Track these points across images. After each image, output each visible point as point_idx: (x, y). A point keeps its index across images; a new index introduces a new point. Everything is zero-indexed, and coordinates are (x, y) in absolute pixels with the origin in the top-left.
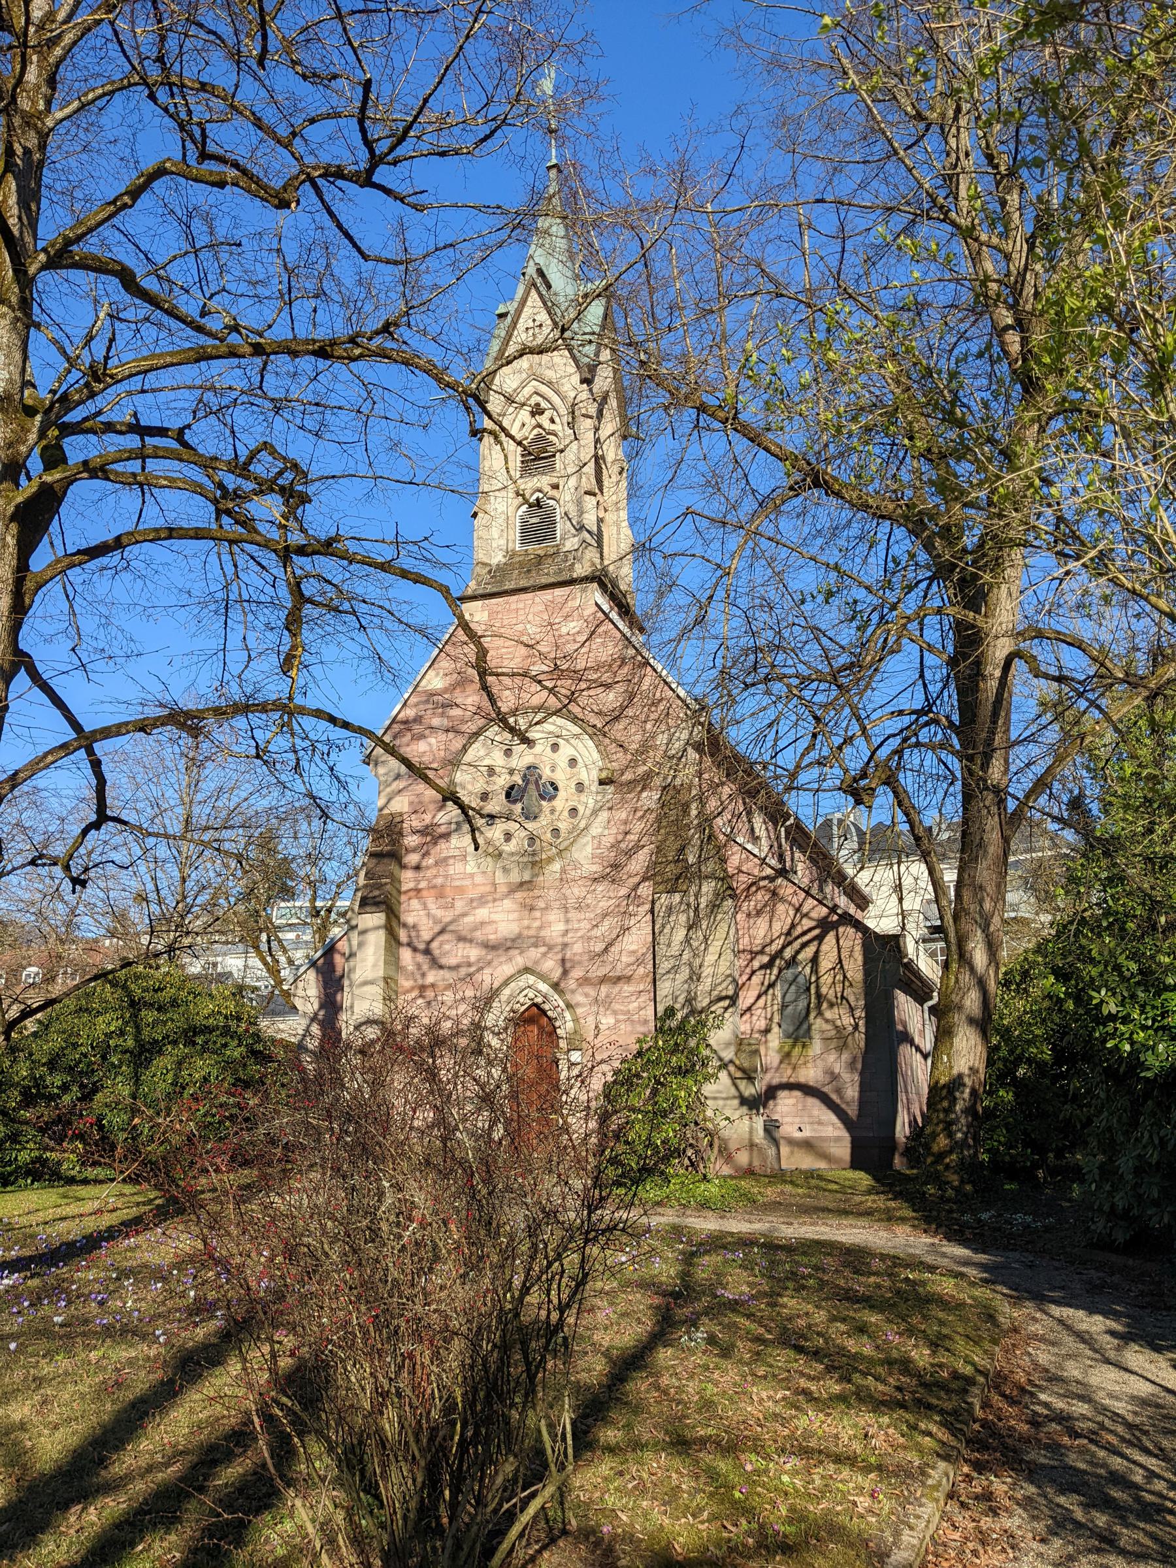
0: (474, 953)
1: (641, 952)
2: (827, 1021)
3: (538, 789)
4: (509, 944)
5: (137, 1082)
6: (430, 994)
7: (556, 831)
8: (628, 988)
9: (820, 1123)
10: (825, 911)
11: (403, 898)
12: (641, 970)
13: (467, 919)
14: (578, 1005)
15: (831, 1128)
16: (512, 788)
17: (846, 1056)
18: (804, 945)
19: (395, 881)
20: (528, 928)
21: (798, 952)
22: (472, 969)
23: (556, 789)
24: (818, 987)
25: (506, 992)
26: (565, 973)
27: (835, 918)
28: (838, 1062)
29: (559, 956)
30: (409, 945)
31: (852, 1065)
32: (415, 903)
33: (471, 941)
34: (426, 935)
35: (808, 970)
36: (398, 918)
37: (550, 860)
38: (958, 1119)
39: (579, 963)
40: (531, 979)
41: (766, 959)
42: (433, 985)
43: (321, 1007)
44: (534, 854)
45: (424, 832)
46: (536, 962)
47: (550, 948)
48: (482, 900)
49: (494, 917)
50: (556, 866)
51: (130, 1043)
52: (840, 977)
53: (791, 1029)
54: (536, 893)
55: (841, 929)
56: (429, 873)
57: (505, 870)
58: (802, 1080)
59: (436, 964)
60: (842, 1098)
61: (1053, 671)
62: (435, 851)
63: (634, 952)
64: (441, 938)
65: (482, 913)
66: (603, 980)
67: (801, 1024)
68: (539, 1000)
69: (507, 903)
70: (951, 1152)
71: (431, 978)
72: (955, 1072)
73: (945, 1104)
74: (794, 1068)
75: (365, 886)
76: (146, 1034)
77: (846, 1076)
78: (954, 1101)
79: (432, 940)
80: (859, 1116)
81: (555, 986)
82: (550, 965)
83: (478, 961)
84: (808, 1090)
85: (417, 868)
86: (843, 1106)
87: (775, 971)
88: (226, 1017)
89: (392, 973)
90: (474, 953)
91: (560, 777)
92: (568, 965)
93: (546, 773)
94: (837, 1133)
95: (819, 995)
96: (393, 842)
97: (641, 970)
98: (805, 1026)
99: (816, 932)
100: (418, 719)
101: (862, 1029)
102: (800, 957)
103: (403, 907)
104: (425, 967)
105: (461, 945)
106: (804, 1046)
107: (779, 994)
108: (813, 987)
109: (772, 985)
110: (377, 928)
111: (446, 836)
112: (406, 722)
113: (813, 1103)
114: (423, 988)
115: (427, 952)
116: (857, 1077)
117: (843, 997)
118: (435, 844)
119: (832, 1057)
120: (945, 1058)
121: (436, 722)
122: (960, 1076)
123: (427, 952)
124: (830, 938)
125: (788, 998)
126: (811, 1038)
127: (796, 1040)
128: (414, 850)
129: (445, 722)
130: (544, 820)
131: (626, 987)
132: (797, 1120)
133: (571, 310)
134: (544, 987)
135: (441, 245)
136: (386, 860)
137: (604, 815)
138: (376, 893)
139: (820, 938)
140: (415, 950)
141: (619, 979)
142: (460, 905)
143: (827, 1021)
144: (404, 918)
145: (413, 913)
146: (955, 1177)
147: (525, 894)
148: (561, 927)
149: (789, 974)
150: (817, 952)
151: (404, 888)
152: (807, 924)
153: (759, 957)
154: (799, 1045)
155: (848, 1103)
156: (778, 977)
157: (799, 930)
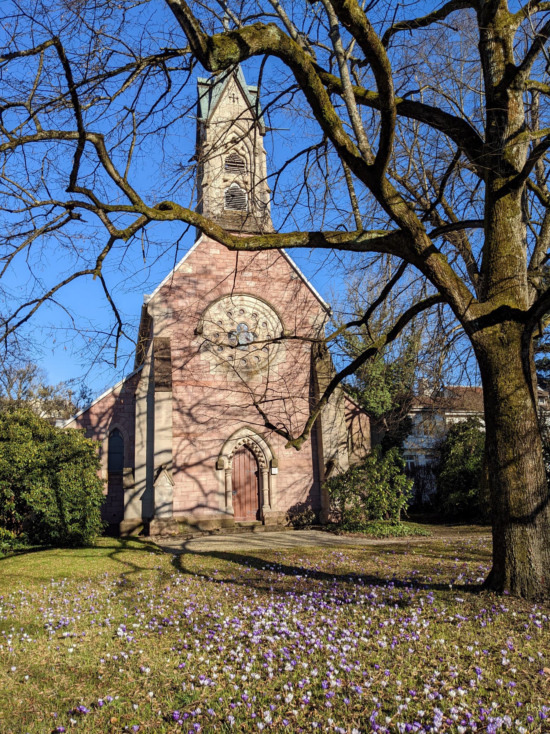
0: (217, 415)
2: (356, 455)
10: (354, 407)
14: (275, 444)
24: (352, 440)
34: (189, 406)
37: (257, 372)
40: (249, 432)
45: (184, 349)
52: (360, 436)
55: (361, 415)
61: (193, 471)
68: (251, 442)
71: (192, 429)
85: (181, 368)
90: (217, 415)
95: (352, 443)
96: (169, 354)
99: (351, 415)
100: (178, 288)
108: (350, 440)
114: (188, 434)
115: (189, 414)
123: (189, 414)
124: (356, 420)
128: (179, 358)
133: (76, 487)
135: (139, 234)
139: (352, 418)
140: (182, 413)
143: (356, 455)
150: (351, 425)
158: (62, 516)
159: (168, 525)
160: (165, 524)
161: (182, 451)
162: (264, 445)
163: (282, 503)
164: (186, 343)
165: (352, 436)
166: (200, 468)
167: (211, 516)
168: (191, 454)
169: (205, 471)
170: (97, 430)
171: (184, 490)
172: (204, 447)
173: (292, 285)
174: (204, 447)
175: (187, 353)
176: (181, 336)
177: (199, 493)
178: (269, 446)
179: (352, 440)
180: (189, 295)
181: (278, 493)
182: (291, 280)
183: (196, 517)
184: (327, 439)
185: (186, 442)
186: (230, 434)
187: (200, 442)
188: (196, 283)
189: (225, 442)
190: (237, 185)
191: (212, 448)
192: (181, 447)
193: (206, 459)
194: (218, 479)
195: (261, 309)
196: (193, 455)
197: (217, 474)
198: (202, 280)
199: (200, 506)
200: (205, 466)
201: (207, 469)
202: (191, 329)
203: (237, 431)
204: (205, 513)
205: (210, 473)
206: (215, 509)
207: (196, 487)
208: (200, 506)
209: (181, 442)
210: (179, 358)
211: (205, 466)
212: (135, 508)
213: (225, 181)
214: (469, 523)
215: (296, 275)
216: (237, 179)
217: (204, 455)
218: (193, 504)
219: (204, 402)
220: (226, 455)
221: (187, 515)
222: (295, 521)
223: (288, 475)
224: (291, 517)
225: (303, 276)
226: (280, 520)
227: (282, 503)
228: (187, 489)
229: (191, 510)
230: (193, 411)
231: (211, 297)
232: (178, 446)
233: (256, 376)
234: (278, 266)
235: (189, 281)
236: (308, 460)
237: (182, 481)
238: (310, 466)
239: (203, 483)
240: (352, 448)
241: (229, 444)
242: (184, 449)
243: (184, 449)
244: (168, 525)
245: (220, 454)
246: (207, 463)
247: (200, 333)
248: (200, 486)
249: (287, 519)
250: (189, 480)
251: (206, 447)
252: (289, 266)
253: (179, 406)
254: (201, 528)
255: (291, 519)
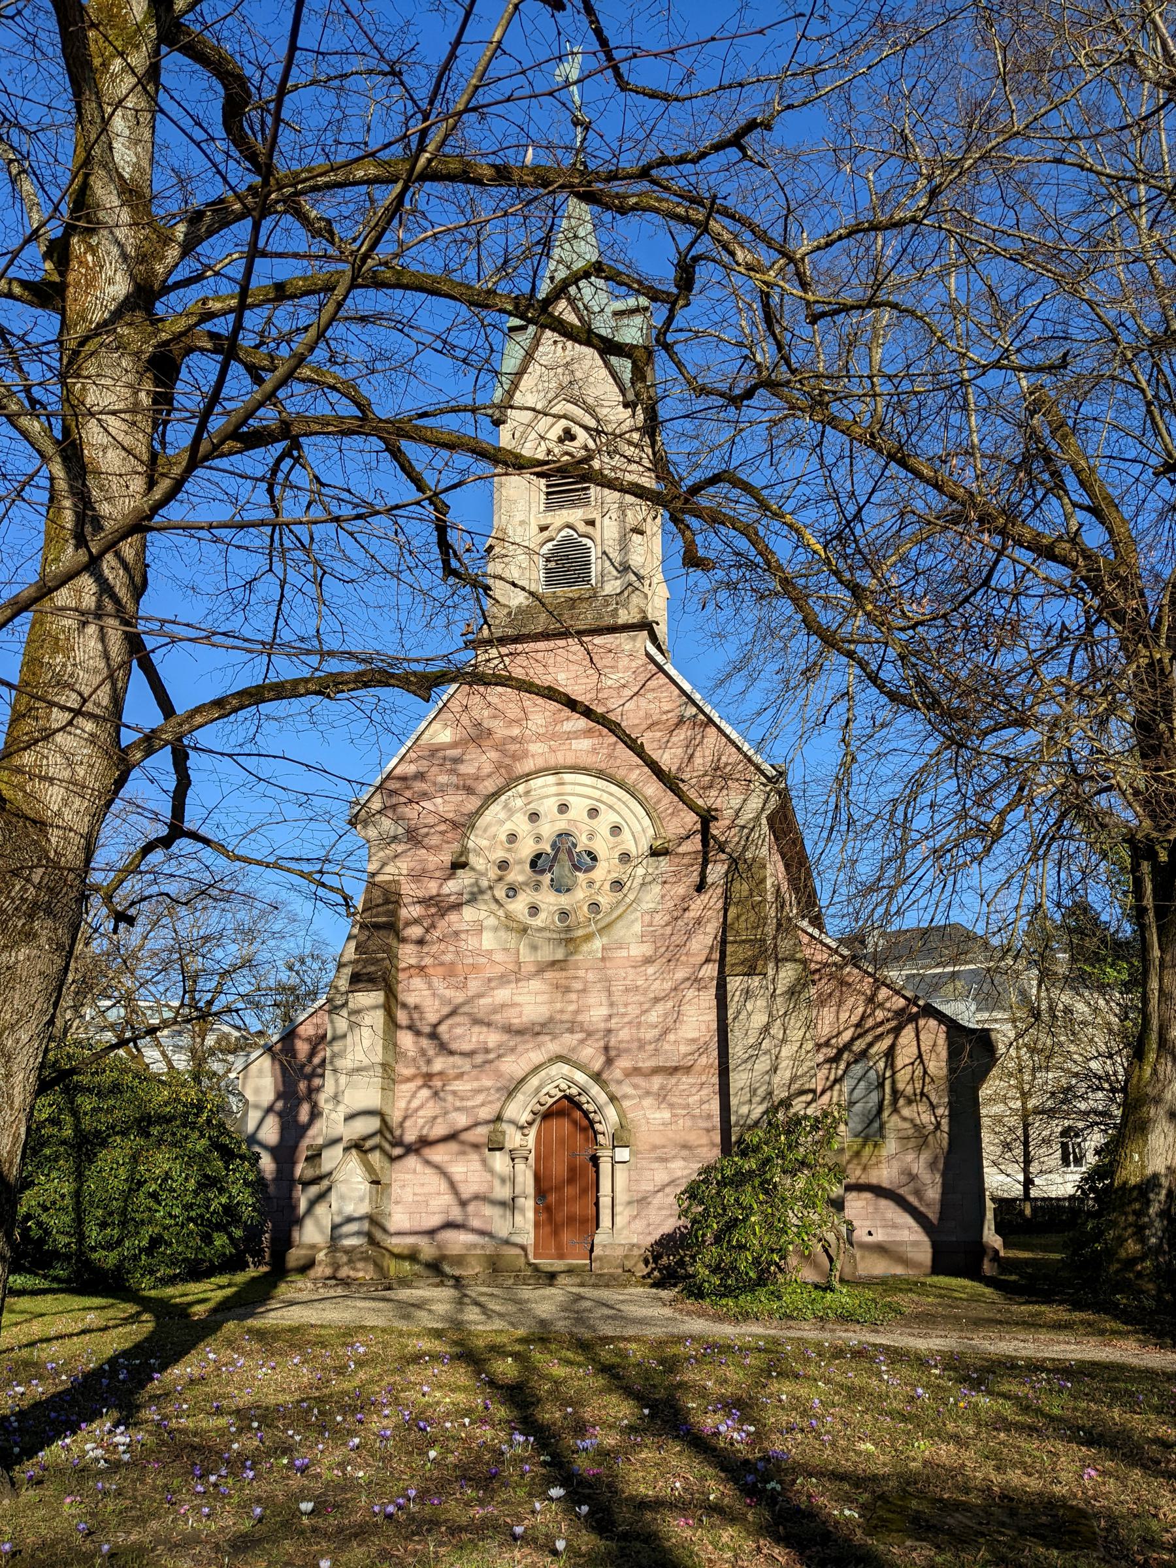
0: (493, 1038)
1: (702, 1040)
2: (904, 1119)
3: (571, 859)
4: (537, 1029)
5: (80, 1177)
6: (437, 1083)
7: (595, 906)
8: (686, 1080)
9: (895, 1226)
10: (902, 1002)
11: (401, 976)
12: (703, 1060)
13: (482, 1001)
14: (625, 1096)
15: (906, 1232)
16: (538, 856)
17: (925, 1156)
18: (879, 1038)
19: (393, 957)
20: (562, 1011)
21: (870, 1045)
22: (491, 1056)
23: (594, 859)
24: (894, 1083)
25: (534, 1081)
26: (609, 1062)
27: (915, 1010)
28: (919, 1164)
29: (602, 1043)
30: (410, 1028)
31: (932, 1165)
32: (417, 982)
33: (489, 1025)
34: (432, 1018)
35: (882, 1064)
36: (396, 998)
37: (588, 938)
38: (1152, 1222)
39: (627, 1050)
40: (566, 1069)
41: (832, 1052)
42: (440, 1073)
43: (279, 1096)
44: (568, 929)
45: (425, 902)
46: (573, 1050)
47: (590, 1034)
48: (503, 980)
49: (517, 999)
50: (597, 944)
51: (68, 1132)
52: (919, 1072)
53: (860, 1128)
54: (571, 973)
56: (434, 949)
57: (534, 948)
58: (874, 1181)
59: (444, 1048)
60: (921, 1199)
61: (437, 1154)
62: (442, 924)
63: (694, 1040)
64: (449, 1022)
65: (502, 994)
66: (656, 1071)
67: (871, 1122)
68: (574, 1091)
69: (536, 984)
70: (1142, 1259)
71: (438, 1065)
72: (1149, 1171)
73: (1137, 1206)
74: (864, 1169)
75: (356, 962)
76: (86, 1123)
77: (926, 1176)
78: (1148, 1203)
79: (439, 1023)
80: (941, 1219)
81: (597, 1077)
82: (591, 1054)
83: (499, 1046)
84: (879, 1191)
85: (421, 942)
86: (922, 1209)
87: (842, 1066)
88: (185, 1106)
89: (391, 1061)
90: (493, 1038)
91: (601, 847)
92: (613, 1053)
93: (583, 842)
94: (914, 1237)
95: (894, 1091)
96: (394, 914)
97: (703, 1060)
98: (876, 1125)
99: (893, 1023)
100: (420, 776)
101: (945, 1126)
102: (873, 1051)
103: (400, 987)
104: (431, 1052)
105: (476, 1029)
106: (875, 1146)
107: (845, 1090)
108: (888, 1083)
109: (837, 1081)
110: (376, 1007)
111: (457, 906)
112: (403, 779)
113: (887, 1206)
114: (429, 1076)
115: (434, 1036)
116: (938, 1178)
117: (922, 1094)
118: (443, 915)
119: (910, 1157)
120: (1136, 1157)
121: (443, 779)
122: (1156, 1176)
123: (434, 1036)
124: (908, 1032)
125: (858, 1094)
126: (883, 1137)
127: (866, 1139)
128: (417, 921)
129: (454, 779)
130: (580, 894)
131: (684, 1079)
132: (868, 1223)
134: (580, 1077)
136: (382, 933)
137: (656, 889)
138: (372, 969)
139: (897, 1031)
140: (418, 1033)
141: (676, 1069)
142: (474, 986)
143: (904, 1119)
144: (402, 997)
145: (414, 991)
146: (1151, 1286)
147: (558, 975)
148: (604, 1011)
149: (858, 1069)
150: (892, 1048)
151: (402, 965)
152: (880, 1015)
153: (824, 1050)
154: (871, 1144)
155: (928, 1205)
156: (845, 1072)
157: (870, 1023)
158: (81, 1237)
159: (350, 1261)
160: (345, 1259)
161: (417, 1110)
162: (602, 1098)
163: (639, 1225)
164: (432, 887)
165: (894, 1073)
166: (453, 1146)
167: (475, 1246)
168: (435, 1118)
169: (464, 1153)
170: (308, 1069)
171: (418, 1190)
172: (465, 1103)
173: (682, 734)
174: (465, 1103)
175: (433, 910)
176: (417, 876)
177: (448, 1199)
178: (613, 1099)
179: (894, 1083)
180: (442, 789)
181: (629, 1203)
182: (681, 721)
183: (439, 1247)
184: (740, 1084)
185: (425, 1093)
186: (520, 1074)
187: (454, 1093)
188: (457, 761)
189: (511, 1094)
190: (572, 532)
191: (483, 1105)
192: (415, 1103)
193: (467, 1129)
194: (491, 1171)
195: (605, 797)
196: (439, 1120)
197: (490, 1161)
198: (473, 753)
199: (449, 1225)
200: (463, 1143)
201: (468, 1149)
202: (447, 858)
203: (536, 1069)
204: (458, 1240)
205: (474, 1157)
206: (482, 1233)
207: (444, 1186)
208: (449, 1225)
209: (415, 1092)
210: (417, 921)
211: (463, 1143)
212: (318, 1224)
213: (543, 529)
214: (1077, 1306)
215: (694, 710)
216: (571, 520)
217: (462, 1120)
218: (435, 1221)
219: (465, 1009)
220: (512, 1122)
221: (422, 1242)
222: (665, 1268)
223: (656, 1165)
224: (657, 1258)
225: (707, 709)
226: (629, 1264)
227: (639, 1225)
228: (426, 1190)
229: (431, 1233)
230: (442, 1029)
231: (489, 786)
232: (409, 1102)
233: (585, 948)
234: (650, 696)
235: (444, 758)
236: (708, 1131)
237: (415, 1171)
238: (713, 1145)
239: (457, 1178)
240: (895, 1101)
241: (520, 1097)
242: (421, 1107)
243: (421, 1107)
244: (350, 1261)
245: (499, 1118)
246: (468, 1136)
247: (464, 865)
248: (453, 1185)
249: (646, 1262)
250: (429, 1171)
251: (469, 1104)
252: (677, 692)
253: (411, 1019)
254: (447, 1269)
255: (655, 1262)
